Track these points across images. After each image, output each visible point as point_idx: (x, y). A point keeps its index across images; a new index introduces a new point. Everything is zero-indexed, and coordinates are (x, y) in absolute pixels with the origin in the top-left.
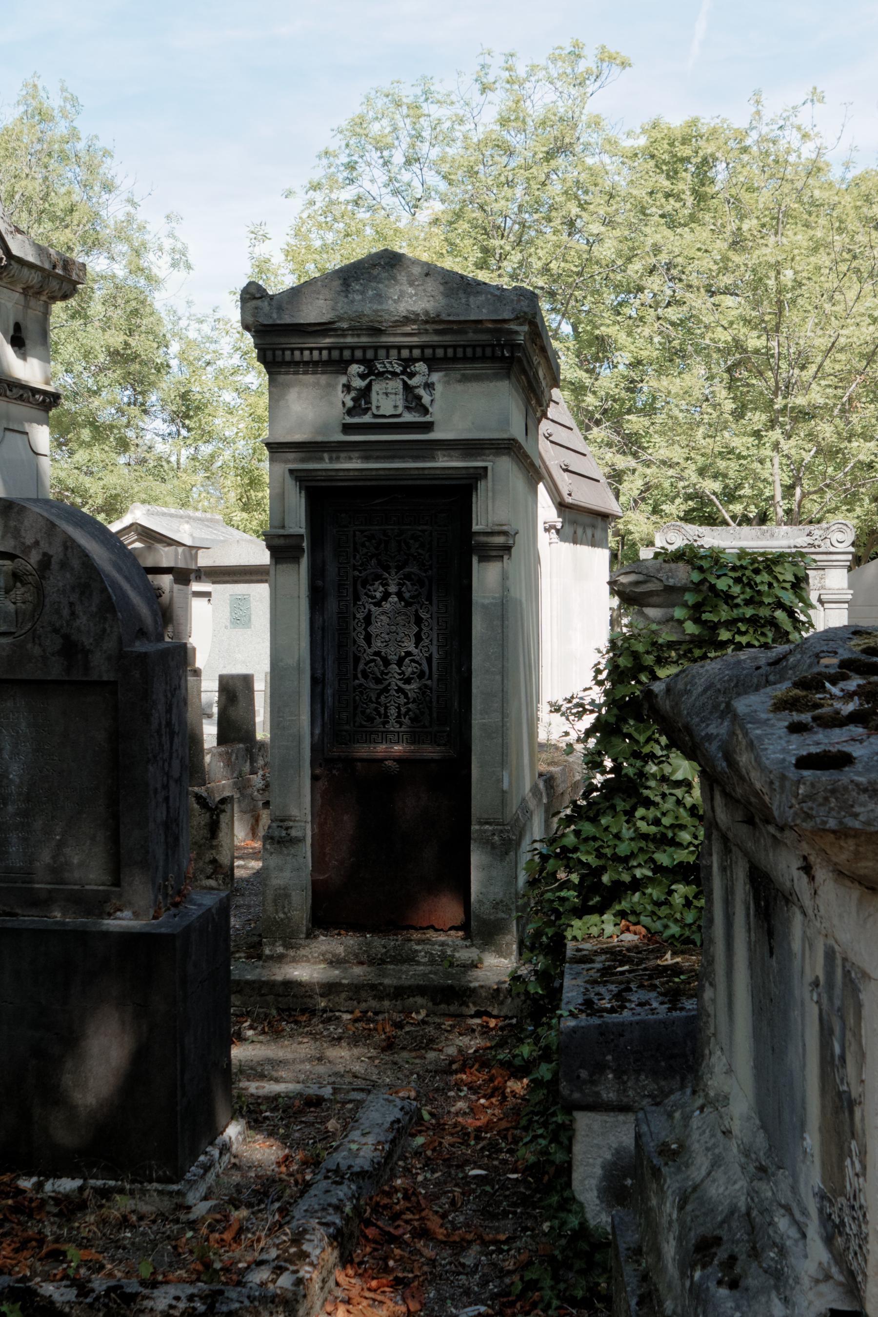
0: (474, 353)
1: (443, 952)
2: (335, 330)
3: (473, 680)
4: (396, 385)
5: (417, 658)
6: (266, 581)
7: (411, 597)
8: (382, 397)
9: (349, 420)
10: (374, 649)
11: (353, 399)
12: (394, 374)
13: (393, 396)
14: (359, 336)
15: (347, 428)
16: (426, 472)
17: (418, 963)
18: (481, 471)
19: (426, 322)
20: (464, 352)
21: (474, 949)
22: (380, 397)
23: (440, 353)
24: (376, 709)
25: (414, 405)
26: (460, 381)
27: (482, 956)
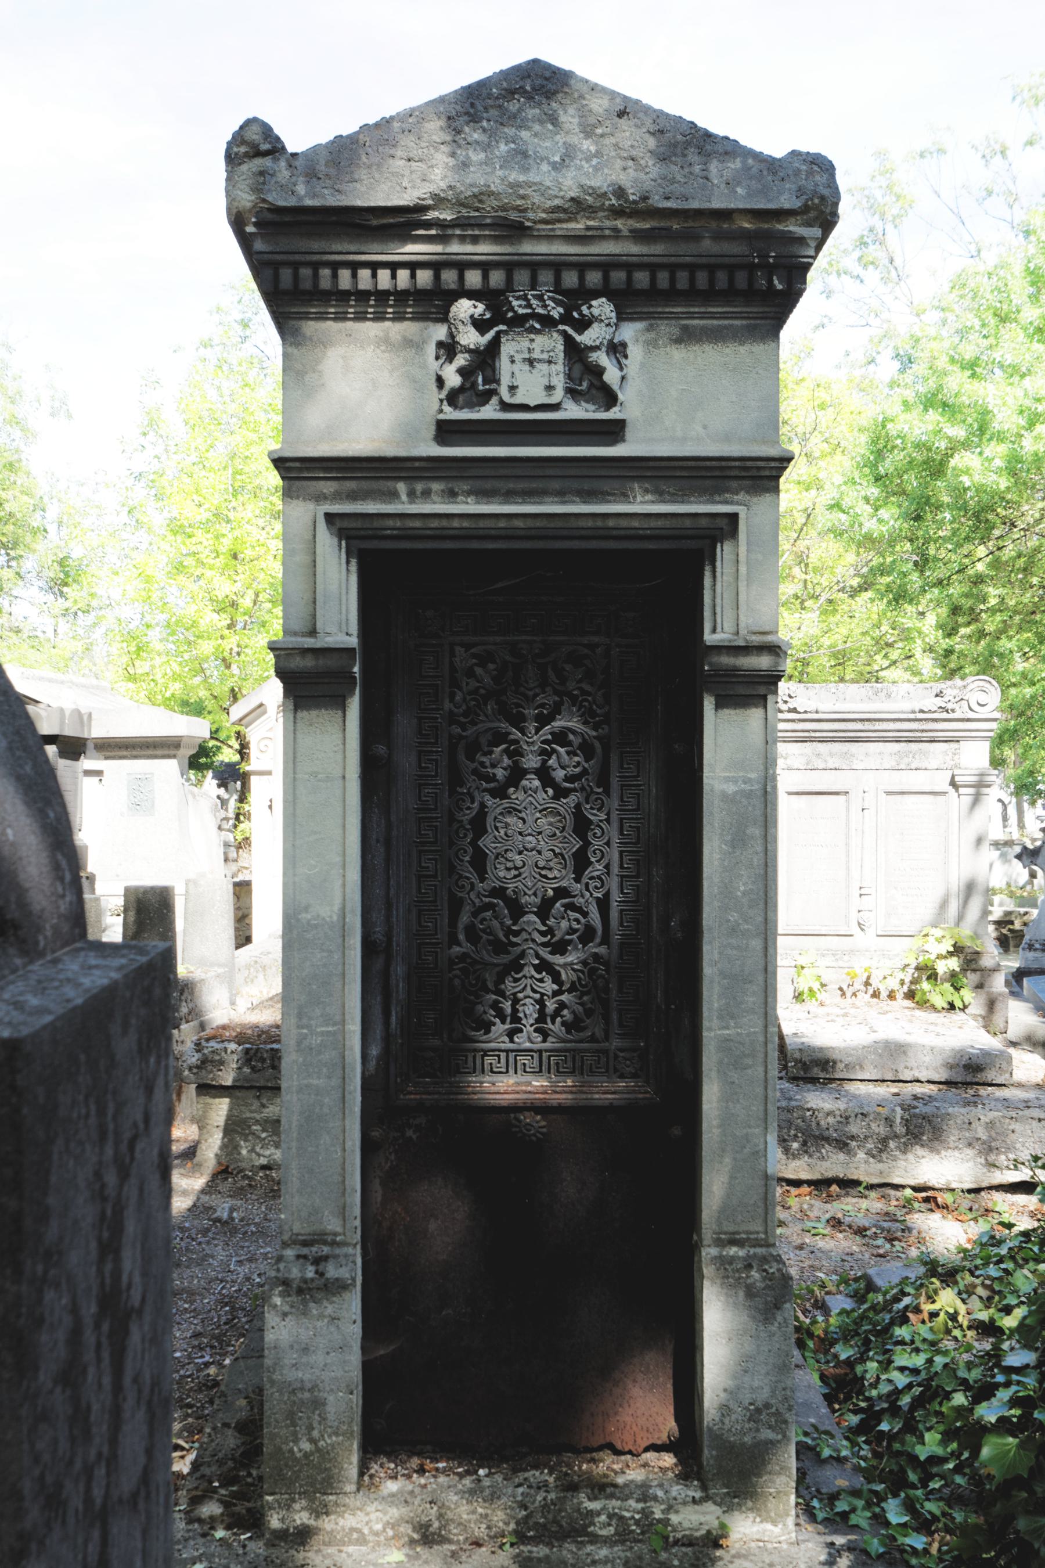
0: (712, 281)
1: (646, 1513)
2: (428, 225)
3: (706, 948)
4: (549, 344)
5: (579, 901)
6: (174, 757)
7: (568, 779)
8: (521, 368)
9: (451, 414)
10: (492, 883)
11: (461, 371)
12: (548, 322)
13: (544, 367)
14: (475, 240)
15: (445, 432)
16: (611, 523)
17: (594, 1539)
18: (723, 523)
19: (617, 213)
20: (692, 280)
21: (710, 1507)
22: (516, 368)
23: (642, 278)
24: (495, 1006)
25: (585, 385)
26: (678, 341)
27: (726, 1519)
